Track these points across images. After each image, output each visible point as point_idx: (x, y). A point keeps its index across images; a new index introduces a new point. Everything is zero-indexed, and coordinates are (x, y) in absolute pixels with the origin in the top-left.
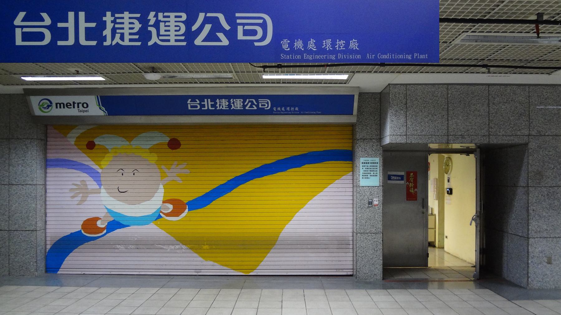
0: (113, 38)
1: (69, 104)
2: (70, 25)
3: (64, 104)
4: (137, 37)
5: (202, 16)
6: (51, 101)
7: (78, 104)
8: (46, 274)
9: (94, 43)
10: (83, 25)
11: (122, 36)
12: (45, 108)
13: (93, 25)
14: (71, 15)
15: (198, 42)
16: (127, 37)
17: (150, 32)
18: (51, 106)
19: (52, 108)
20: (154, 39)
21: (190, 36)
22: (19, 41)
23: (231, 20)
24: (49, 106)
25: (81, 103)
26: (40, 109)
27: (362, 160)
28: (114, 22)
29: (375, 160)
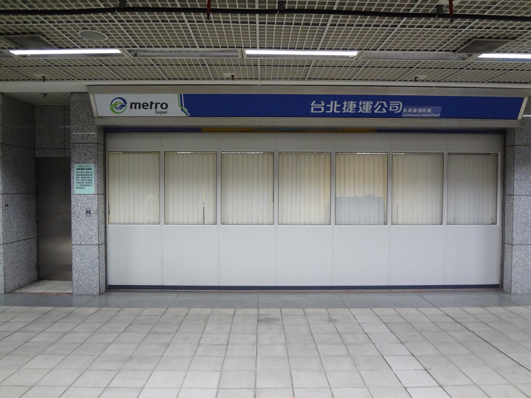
0: (346, 110)
1: (145, 105)
2: (331, 106)
3: (140, 104)
4: (354, 110)
5: (378, 103)
6: (125, 100)
7: (157, 104)
9: (339, 112)
10: (336, 105)
11: (349, 109)
12: (117, 108)
13: (339, 106)
14: (332, 102)
15: (376, 111)
16: (351, 110)
17: (359, 108)
18: (124, 106)
19: (126, 108)
20: (360, 111)
21: (373, 109)
22: (312, 111)
23: (388, 105)
24: (122, 106)
25: (159, 103)
26: (112, 109)
28: (347, 105)
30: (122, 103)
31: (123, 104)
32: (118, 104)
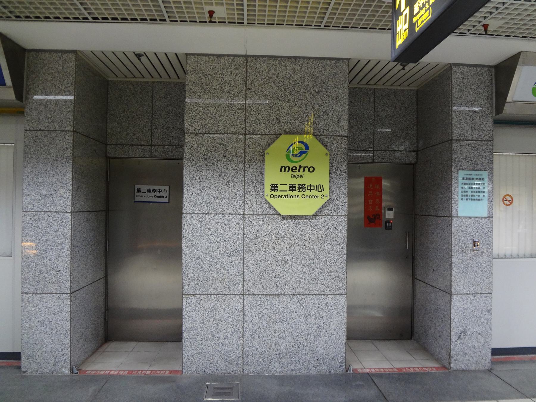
1: (294, 168)
3: (289, 167)
7: (305, 168)
18: (305, 152)
24: (302, 153)
25: (307, 167)
26: (288, 157)
27: (462, 174)
29: (482, 175)
30: (303, 149)
31: (304, 150)
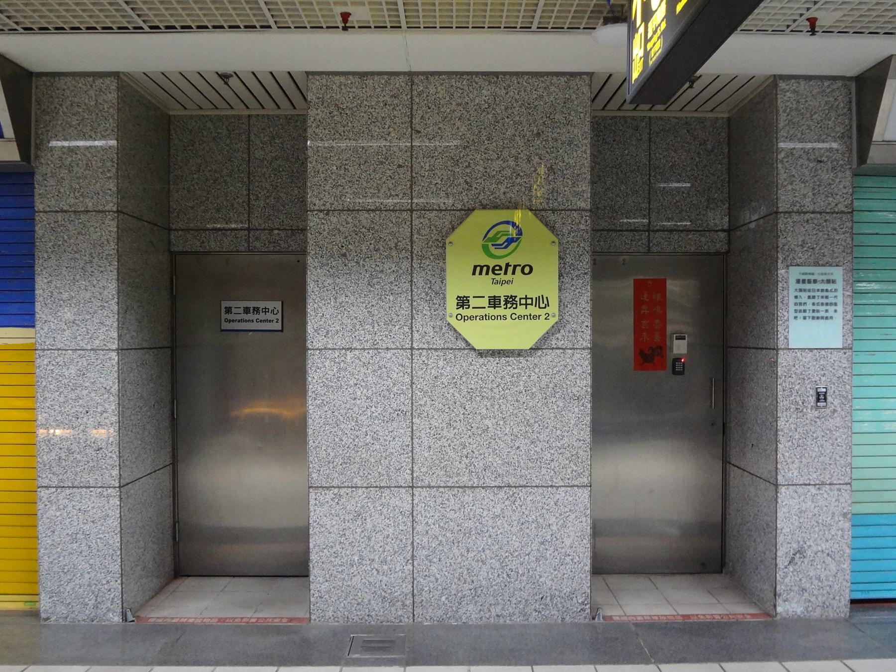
1: (497, 268)
3: (488, 267)
7: (515, 267)
8: (38, 325)
12: (497, 246)
19: (518, 246)
24: (510, 241)
25: (520, 265)
32: (503, 235)
